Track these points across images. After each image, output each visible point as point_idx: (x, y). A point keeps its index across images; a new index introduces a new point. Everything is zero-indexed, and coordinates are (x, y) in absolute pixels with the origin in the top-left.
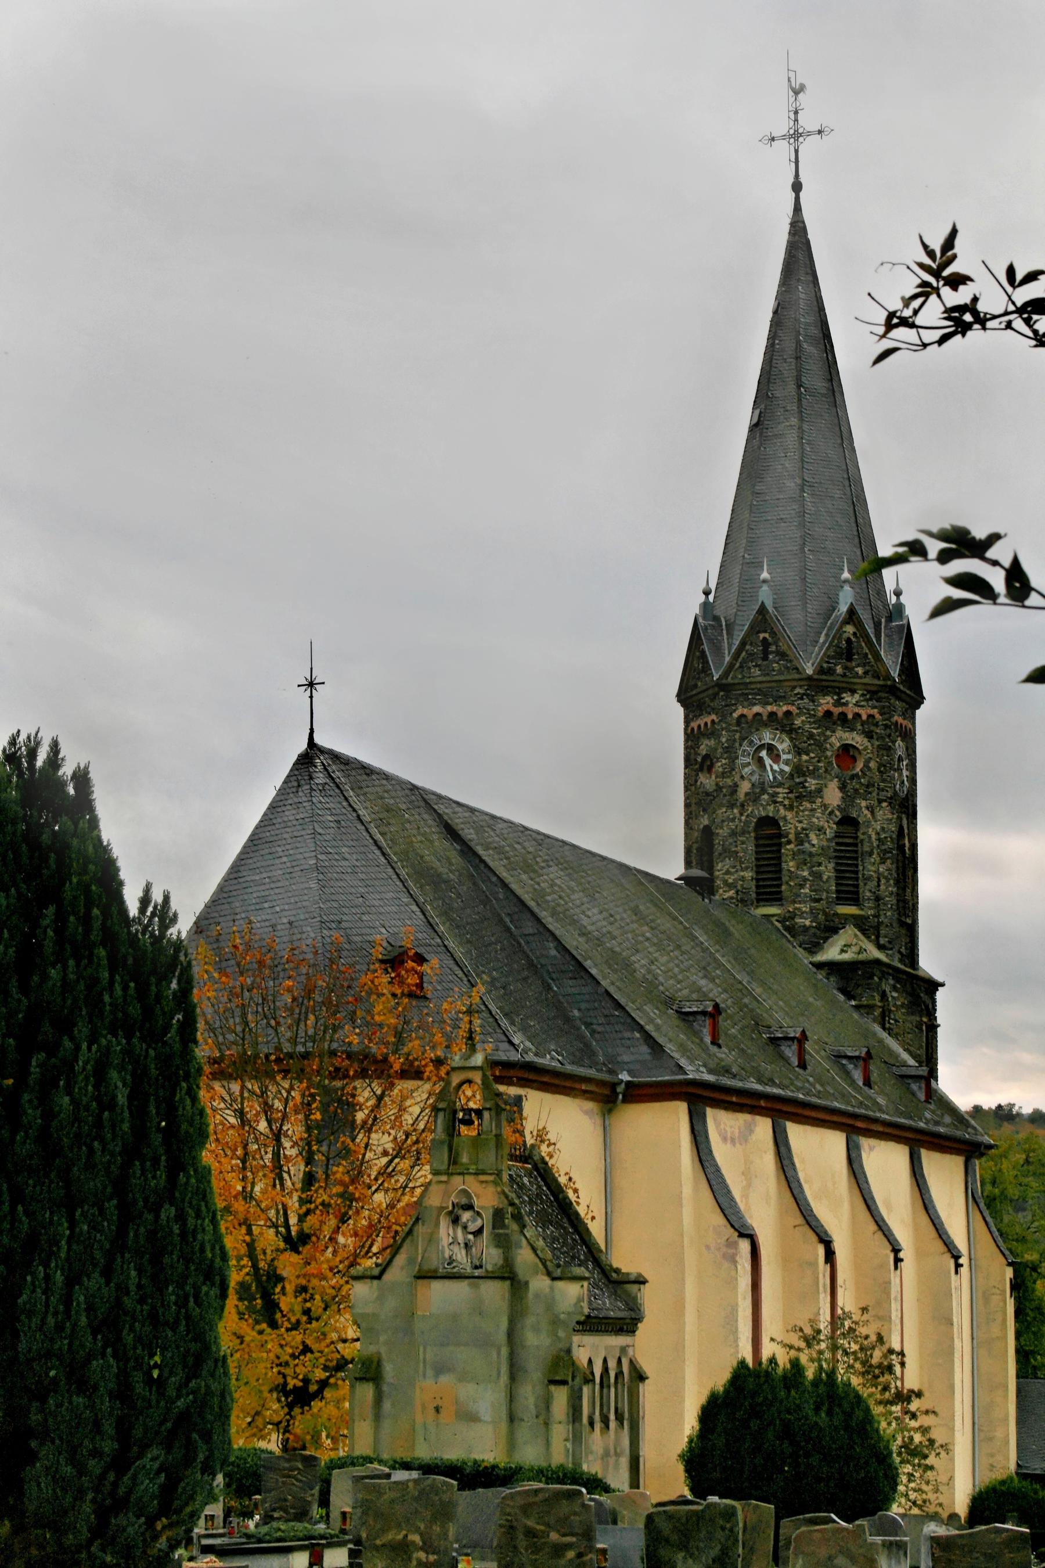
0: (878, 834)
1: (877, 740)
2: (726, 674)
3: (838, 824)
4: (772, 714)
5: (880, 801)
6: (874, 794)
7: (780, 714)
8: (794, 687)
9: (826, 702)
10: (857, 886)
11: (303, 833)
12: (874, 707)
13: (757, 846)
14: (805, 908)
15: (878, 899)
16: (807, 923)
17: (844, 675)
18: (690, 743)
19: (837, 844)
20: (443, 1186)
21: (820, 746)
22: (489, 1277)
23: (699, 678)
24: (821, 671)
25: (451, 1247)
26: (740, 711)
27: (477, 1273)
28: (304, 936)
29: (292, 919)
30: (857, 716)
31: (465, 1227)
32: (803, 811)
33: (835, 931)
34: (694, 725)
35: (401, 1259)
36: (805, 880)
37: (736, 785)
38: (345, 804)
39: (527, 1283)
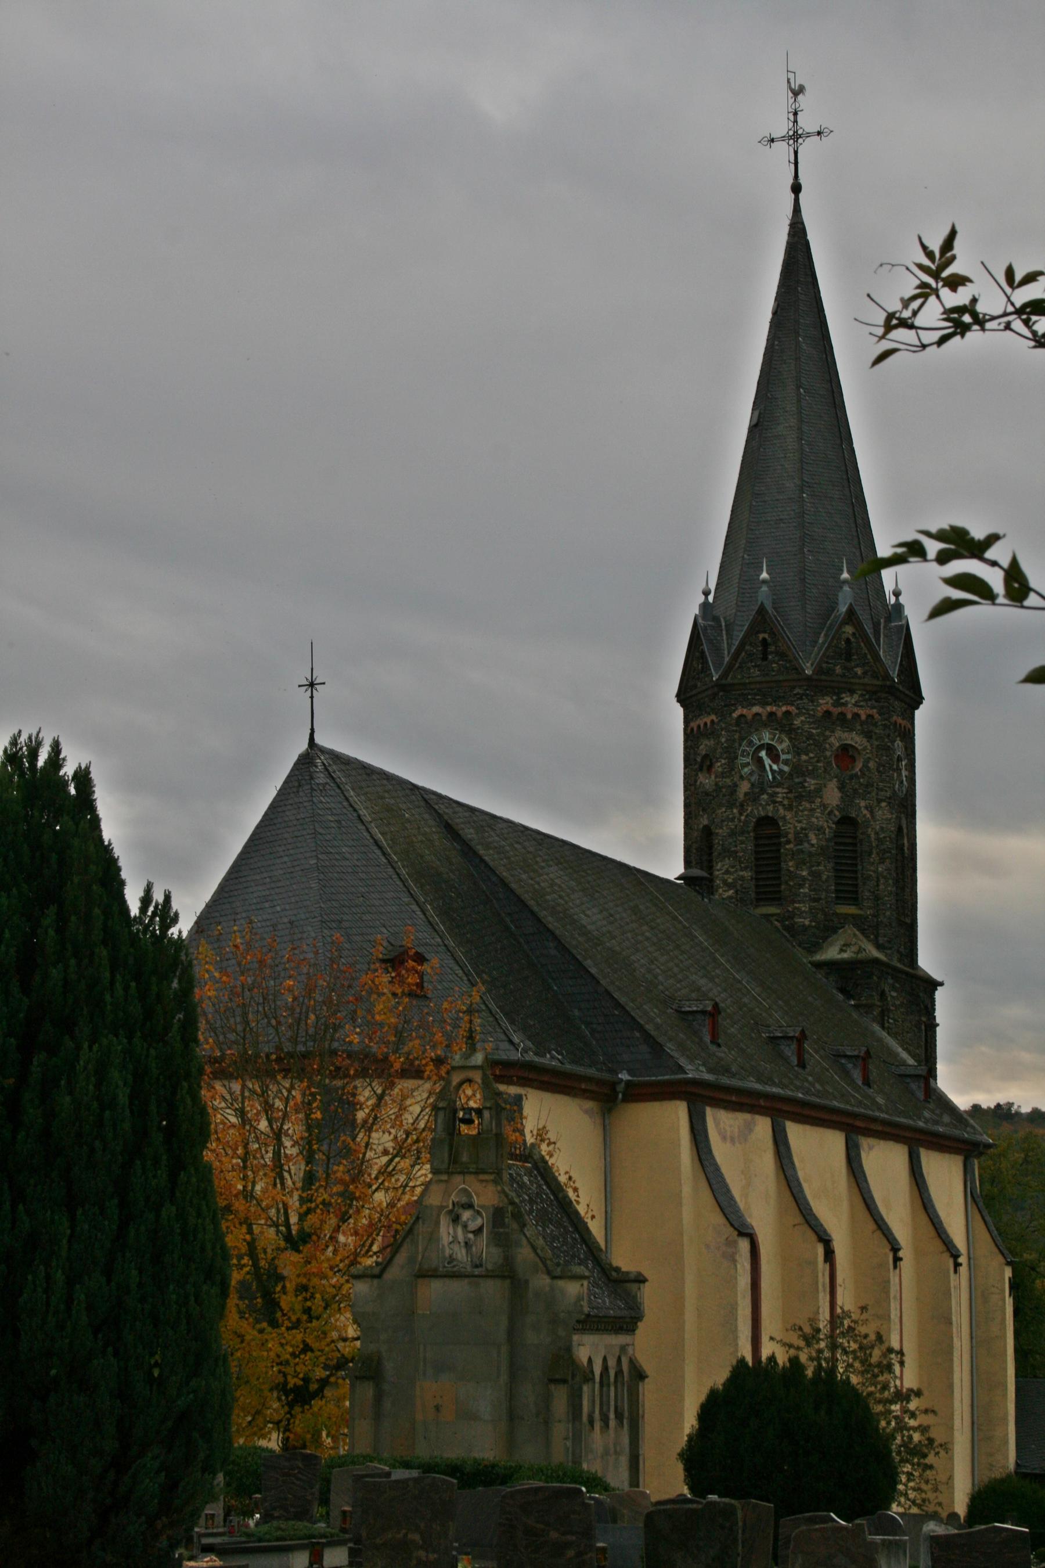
0: (877, 833)
2: (724, 675)
4: (772, 714)
5: (879, 801)
6: (874, 794)
7: (779, 714)
8: (794, 688)
9: (825, 703)
10: (856, 885)
12: (873, 708)
13: (756, 846)
14: (804, 907)
16: (807, 922)
17: (843, 676)
22: (489, 1275)
24: (819, 670)
25: (451, 1246)
27: (477, 1272)
30: (856, 716)
31: (465, 1226)
32: (802, 811)
33: (834, 930)
35: (401, 1258)
36: (804, 879)
37: (736, 785)
38: (345, 804)
39: (527, 1282)
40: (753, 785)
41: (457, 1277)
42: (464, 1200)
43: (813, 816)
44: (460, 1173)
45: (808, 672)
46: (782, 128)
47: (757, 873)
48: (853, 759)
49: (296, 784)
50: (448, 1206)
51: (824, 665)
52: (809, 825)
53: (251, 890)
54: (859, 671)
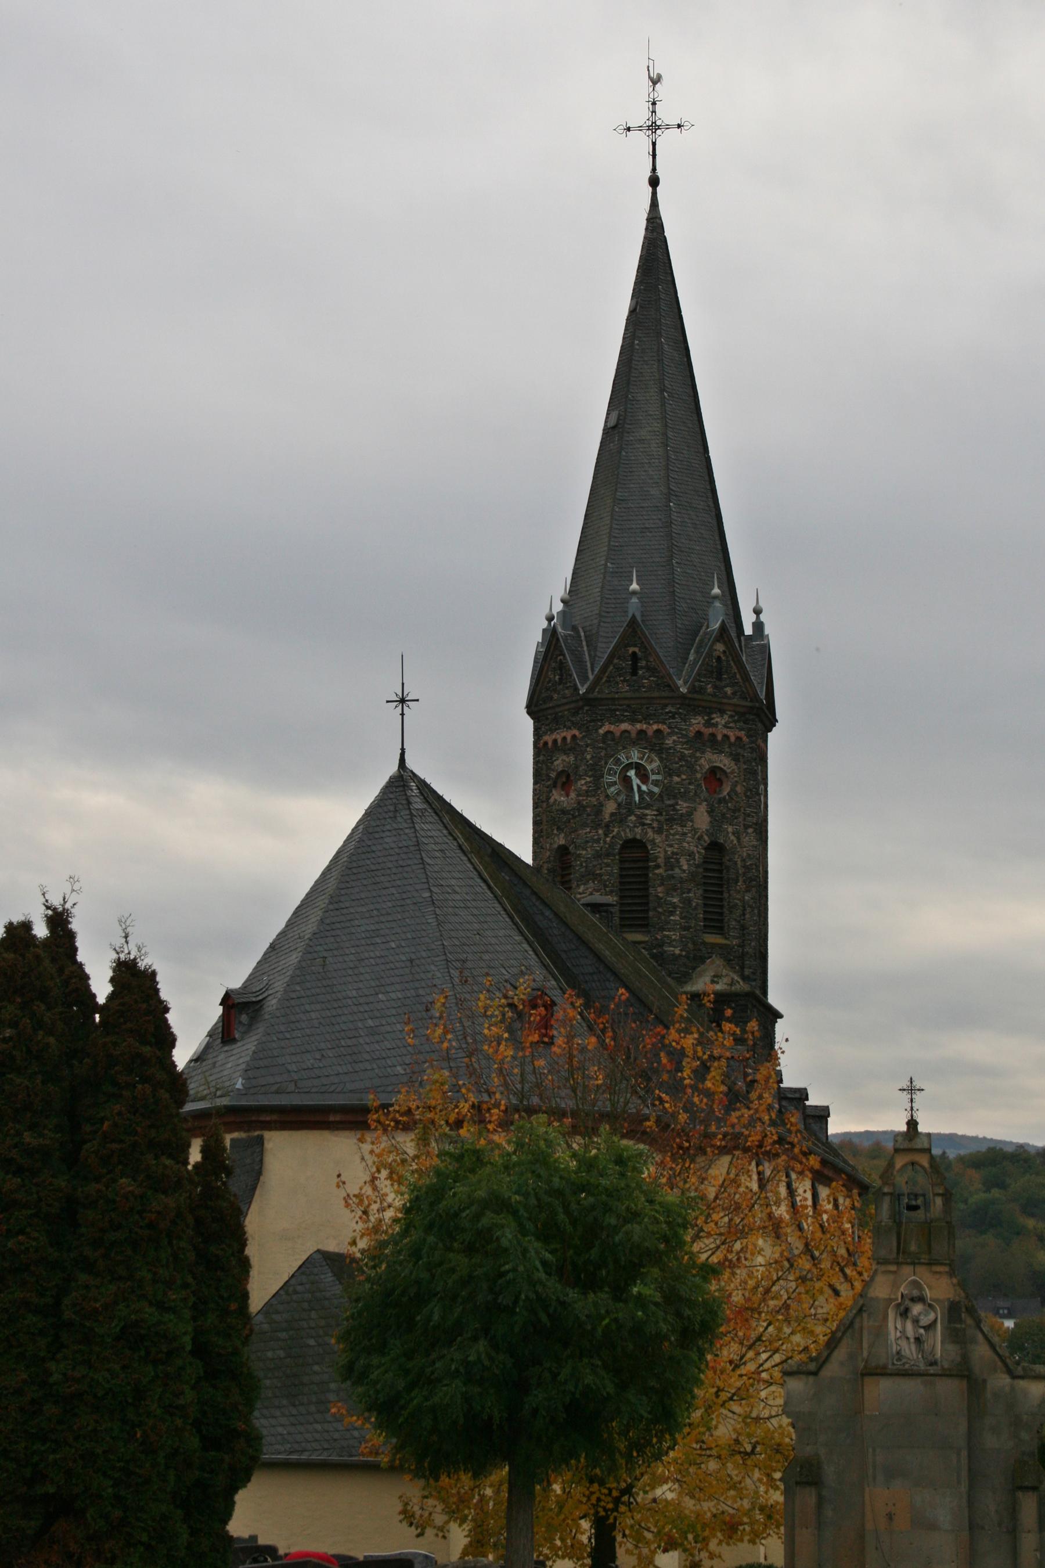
0: (743, 860)
1: (744, 763)
2: (588, 691)
3: (705, 849)
4: (641, 732)
5: (746, 827)
6: (741, 820)
7: (650, 733)
8: (666, 705)
9: (697, 723)
10: (721, 914)
11: (409, 862)
12: (741, 730)
13: (621, 869)
14: (675, 935)
15: (743, 928)
16: (677, 952)
17: (714, 695)
18: (541, 758)
19: (706, 870)
20: (891, 1277)
21: (691, 767)
22: (945, 1374)
23: (555, 691)
24: (693, 690)
25: (899, 1342)
26: (606, 727)
27: (932, 1370)
28: (429, 975)
29: (413, 956)
30: (726, 737)
31: (916, 1321)
32: (673, 835)
33: (702, 960)
34: (549, 738)
35: (840, 1354)
36: (675, 907)
37: (601, 805)
38: (445, 832)
39: (984, 1381)
40: (619, 805)
41: (909, 1375)
42: (915, 1293)
43: (684, 840)
44: (907, 1264)
45: (684, 690)
46: (642, 117)
47: (622, 897)
48: (720, 782)
49: (392, 808)
50: (897, 1299)
51: (697, 684)
52: (677, 849)
53: (357, 922)
54: (729, 690)
